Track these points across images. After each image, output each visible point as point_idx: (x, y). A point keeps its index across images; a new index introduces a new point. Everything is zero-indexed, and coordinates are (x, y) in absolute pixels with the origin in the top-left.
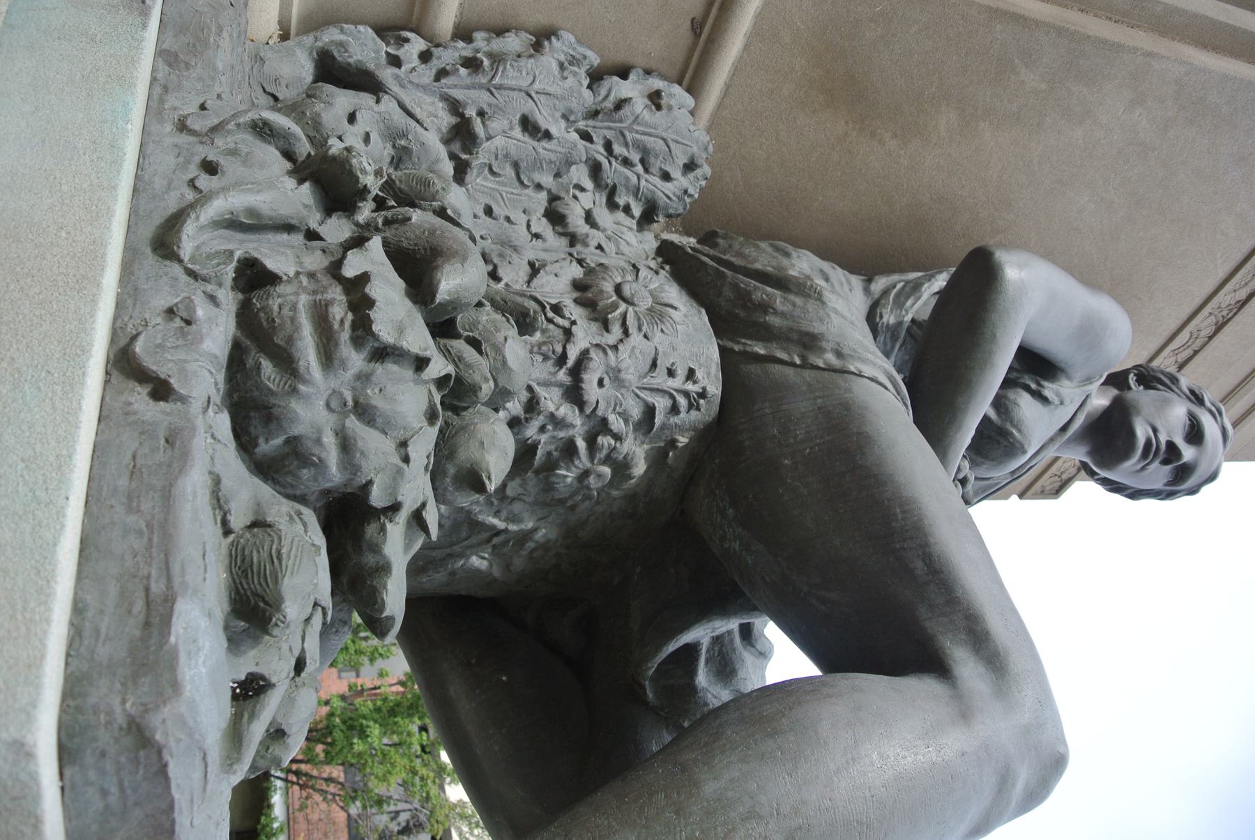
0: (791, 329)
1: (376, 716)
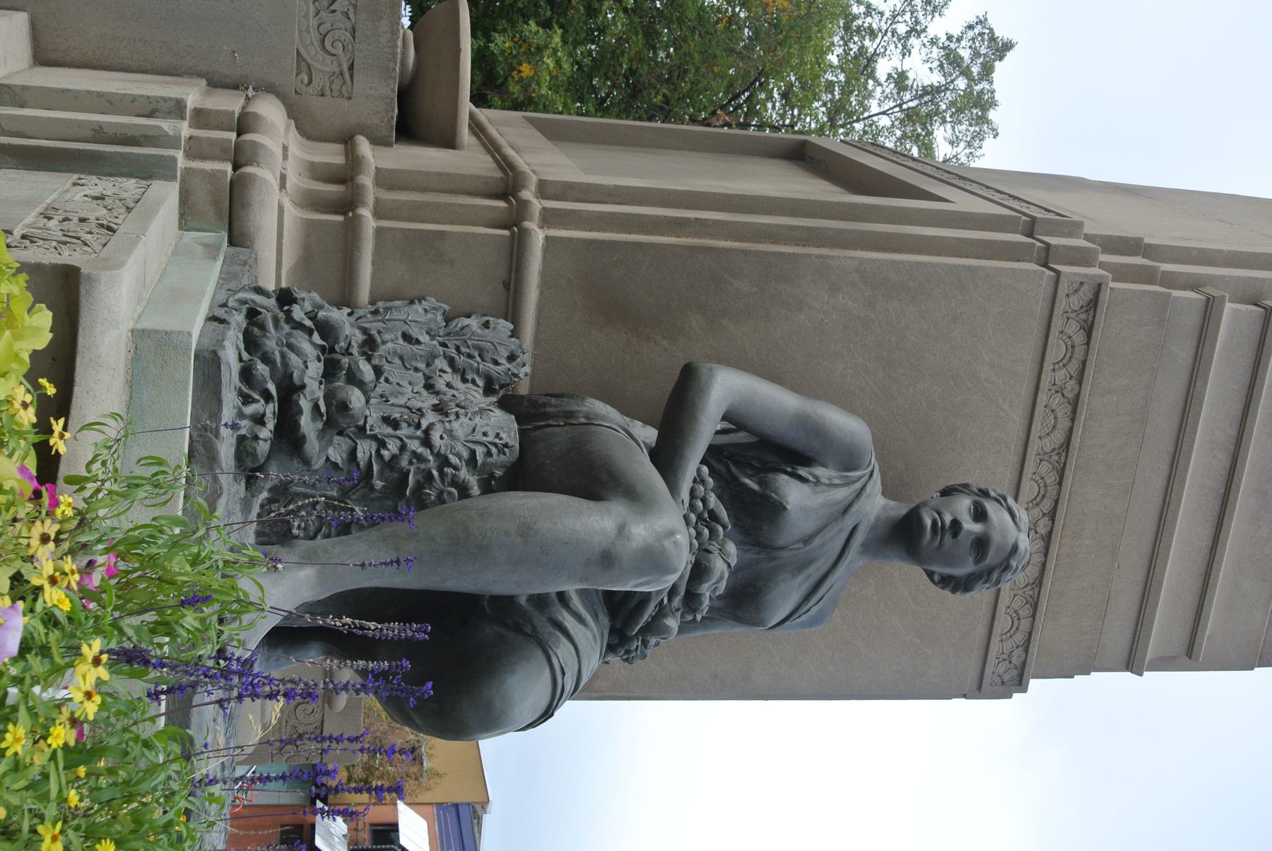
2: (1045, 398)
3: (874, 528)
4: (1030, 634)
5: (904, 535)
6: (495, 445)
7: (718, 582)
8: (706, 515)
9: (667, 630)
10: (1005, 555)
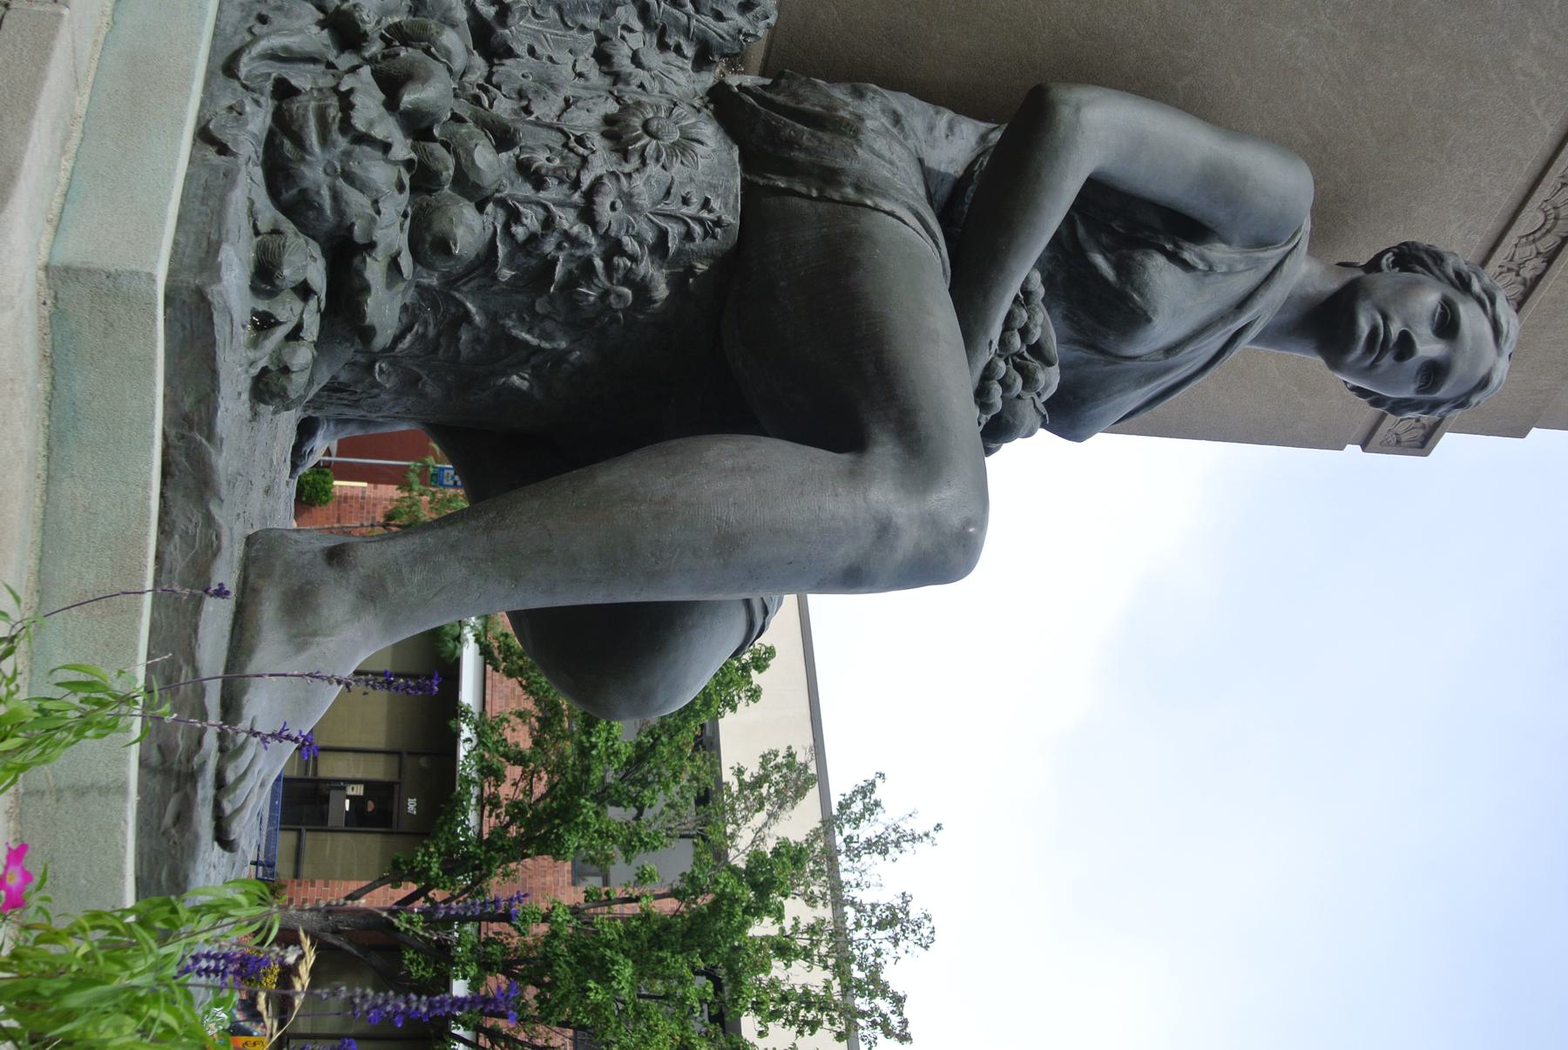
1: (626, 944)
6: (701, 221)
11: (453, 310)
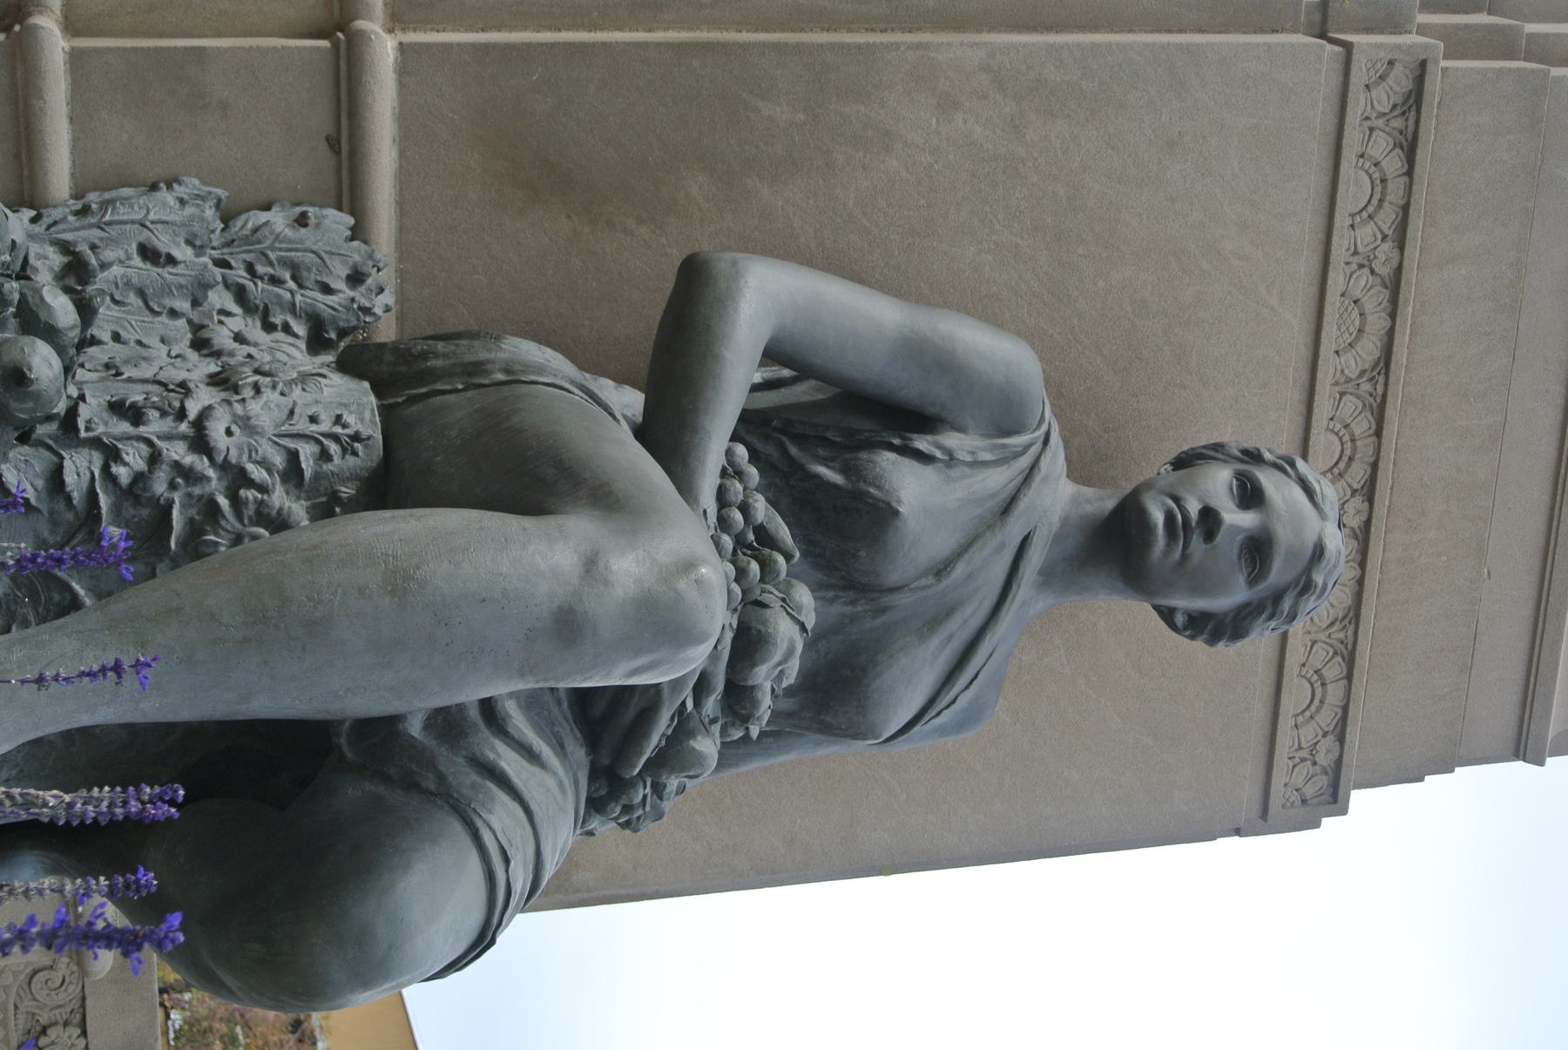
0: (455, 365)
2: (1341, 279)
3: (1059, 538)
4: (1345, 709)
5: (1116, 545)
6: (336, 438)
7: (785, 660)
8: (751, 537)
9: (698, 759)
10: (1301, 565)
11: (57, 597)
